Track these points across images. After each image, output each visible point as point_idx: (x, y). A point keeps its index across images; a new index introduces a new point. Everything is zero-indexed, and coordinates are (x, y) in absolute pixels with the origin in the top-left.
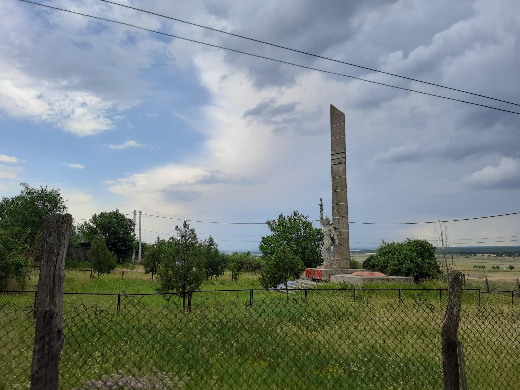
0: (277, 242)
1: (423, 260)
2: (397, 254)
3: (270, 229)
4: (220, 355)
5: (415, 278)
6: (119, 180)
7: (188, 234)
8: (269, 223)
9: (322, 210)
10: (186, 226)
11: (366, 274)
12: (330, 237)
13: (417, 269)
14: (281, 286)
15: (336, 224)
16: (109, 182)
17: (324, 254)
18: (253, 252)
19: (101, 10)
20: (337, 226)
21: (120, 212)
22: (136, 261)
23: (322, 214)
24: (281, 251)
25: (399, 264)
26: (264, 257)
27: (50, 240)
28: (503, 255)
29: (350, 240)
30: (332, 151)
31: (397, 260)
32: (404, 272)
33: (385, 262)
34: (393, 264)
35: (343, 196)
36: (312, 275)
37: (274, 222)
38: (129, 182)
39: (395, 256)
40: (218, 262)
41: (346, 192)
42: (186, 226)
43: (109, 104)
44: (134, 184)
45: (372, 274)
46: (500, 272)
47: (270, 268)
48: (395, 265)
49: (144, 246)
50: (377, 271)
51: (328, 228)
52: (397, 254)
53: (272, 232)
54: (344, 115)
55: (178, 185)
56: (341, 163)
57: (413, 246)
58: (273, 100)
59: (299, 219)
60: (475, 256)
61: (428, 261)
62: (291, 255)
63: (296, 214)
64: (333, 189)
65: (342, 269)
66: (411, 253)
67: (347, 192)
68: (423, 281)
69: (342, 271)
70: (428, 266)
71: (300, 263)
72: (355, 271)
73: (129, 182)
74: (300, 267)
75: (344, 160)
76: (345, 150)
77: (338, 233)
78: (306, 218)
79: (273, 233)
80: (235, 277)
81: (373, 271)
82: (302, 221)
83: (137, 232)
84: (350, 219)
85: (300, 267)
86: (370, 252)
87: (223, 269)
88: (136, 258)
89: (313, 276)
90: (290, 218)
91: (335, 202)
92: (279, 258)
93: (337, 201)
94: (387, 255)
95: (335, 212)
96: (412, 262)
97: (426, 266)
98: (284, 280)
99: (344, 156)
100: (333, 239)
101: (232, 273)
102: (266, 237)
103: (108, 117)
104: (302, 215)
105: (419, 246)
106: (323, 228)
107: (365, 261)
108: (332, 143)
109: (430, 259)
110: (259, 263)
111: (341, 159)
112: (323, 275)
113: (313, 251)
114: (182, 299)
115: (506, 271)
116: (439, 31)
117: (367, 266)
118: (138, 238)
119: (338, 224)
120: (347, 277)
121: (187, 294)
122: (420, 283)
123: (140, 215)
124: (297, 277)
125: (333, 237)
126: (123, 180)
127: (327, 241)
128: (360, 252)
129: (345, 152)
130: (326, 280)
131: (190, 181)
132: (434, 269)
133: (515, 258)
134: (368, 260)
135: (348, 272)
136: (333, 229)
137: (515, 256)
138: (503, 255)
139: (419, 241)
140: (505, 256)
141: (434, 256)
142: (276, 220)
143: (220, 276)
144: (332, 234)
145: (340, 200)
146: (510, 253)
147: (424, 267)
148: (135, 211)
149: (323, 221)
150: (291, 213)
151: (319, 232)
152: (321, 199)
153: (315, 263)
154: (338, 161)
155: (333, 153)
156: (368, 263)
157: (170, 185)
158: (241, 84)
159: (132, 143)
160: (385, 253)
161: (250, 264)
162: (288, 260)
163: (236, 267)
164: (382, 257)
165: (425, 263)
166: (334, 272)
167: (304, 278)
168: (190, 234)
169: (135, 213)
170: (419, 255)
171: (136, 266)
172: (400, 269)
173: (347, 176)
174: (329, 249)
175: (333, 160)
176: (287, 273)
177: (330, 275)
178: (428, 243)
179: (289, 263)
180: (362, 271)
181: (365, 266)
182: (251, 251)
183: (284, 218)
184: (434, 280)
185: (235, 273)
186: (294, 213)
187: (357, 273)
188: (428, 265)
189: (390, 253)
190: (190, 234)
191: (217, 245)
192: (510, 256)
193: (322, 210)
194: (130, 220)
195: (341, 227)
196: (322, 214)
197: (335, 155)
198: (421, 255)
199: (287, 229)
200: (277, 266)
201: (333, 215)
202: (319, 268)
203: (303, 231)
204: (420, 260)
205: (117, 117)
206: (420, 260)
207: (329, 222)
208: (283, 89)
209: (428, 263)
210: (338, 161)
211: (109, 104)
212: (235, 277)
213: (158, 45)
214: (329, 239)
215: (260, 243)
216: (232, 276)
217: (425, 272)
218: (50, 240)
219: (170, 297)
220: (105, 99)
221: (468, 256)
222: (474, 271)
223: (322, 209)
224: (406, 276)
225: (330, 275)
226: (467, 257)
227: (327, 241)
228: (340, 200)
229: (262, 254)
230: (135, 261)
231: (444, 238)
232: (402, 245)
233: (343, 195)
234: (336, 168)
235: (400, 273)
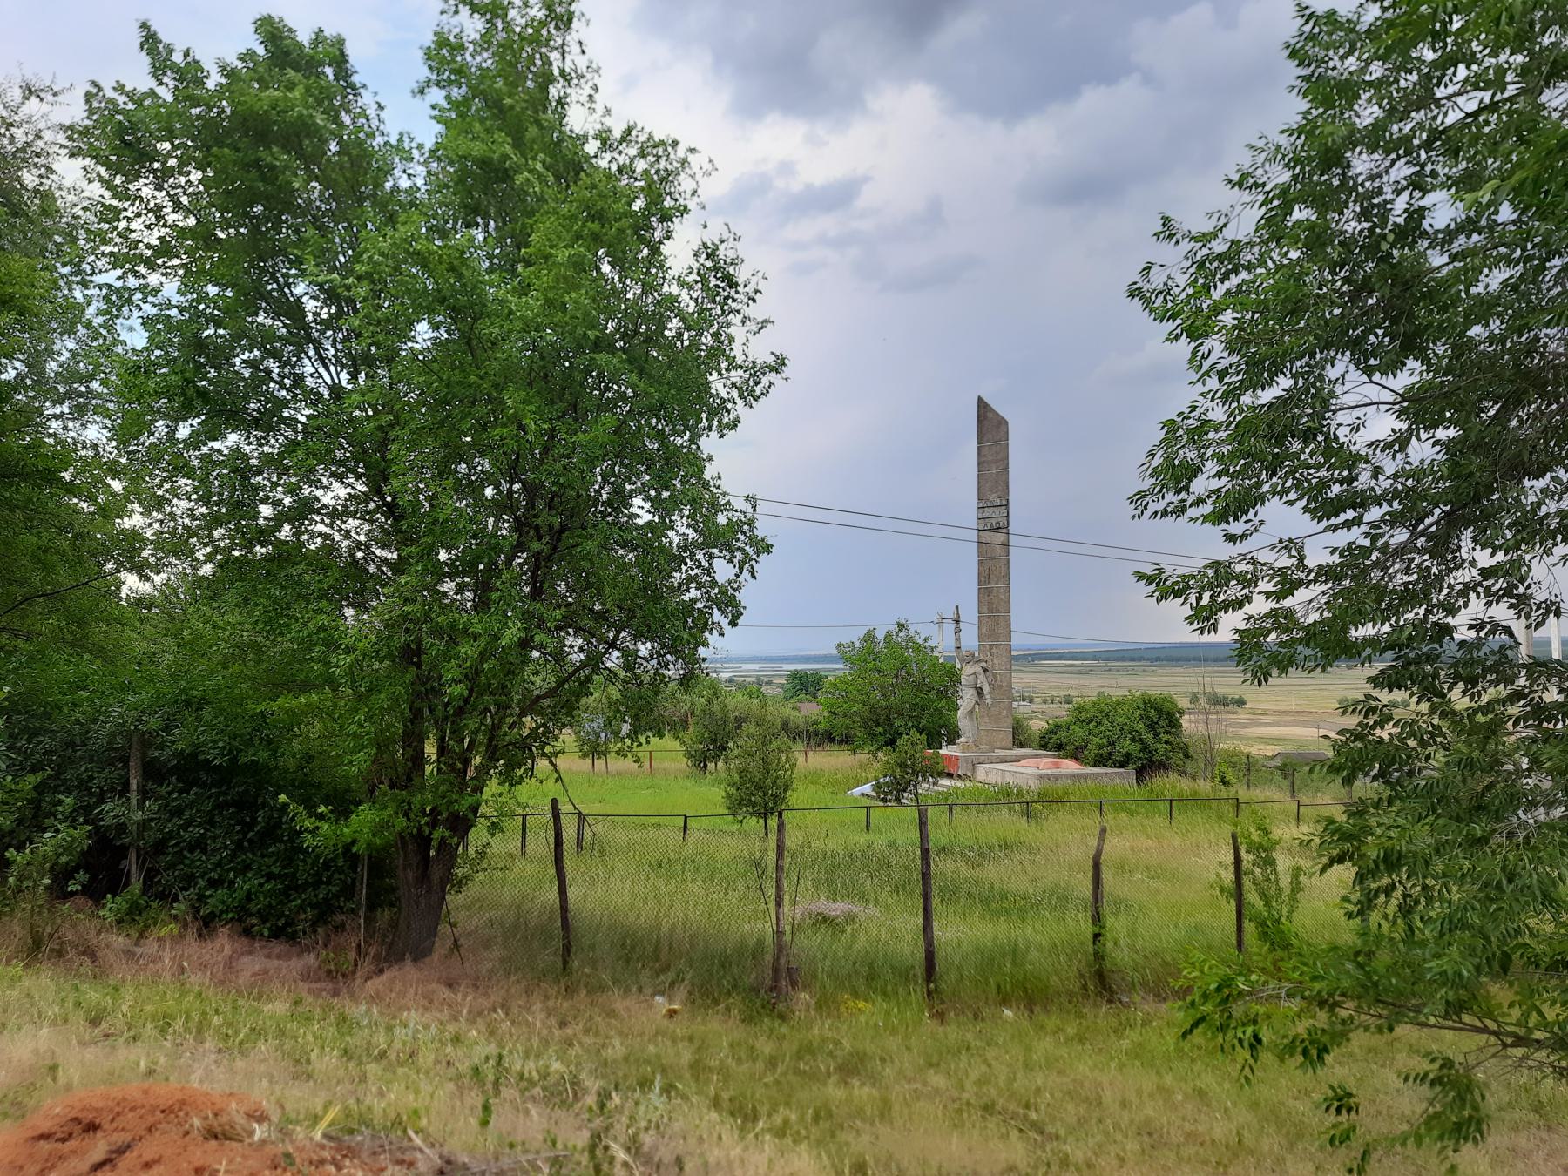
1: (1156, 735)
17: (962, 719)
23: (958, 640)
39: (1102, 728)
45: (1057, 765)
48: (1101, 746)
61: (1165, 737)
63: (901, 627)
64: (979, 582)
95: (984, 631)
96: (1133, 740)
100: (980, 692)
114: (762, 821)
174: (971, 712)
184: (1173, 777)
198: (1152, 727)
204: (1148, 737)
206: (1148, 737)
209: (1166, 742)
214: (972, 692)
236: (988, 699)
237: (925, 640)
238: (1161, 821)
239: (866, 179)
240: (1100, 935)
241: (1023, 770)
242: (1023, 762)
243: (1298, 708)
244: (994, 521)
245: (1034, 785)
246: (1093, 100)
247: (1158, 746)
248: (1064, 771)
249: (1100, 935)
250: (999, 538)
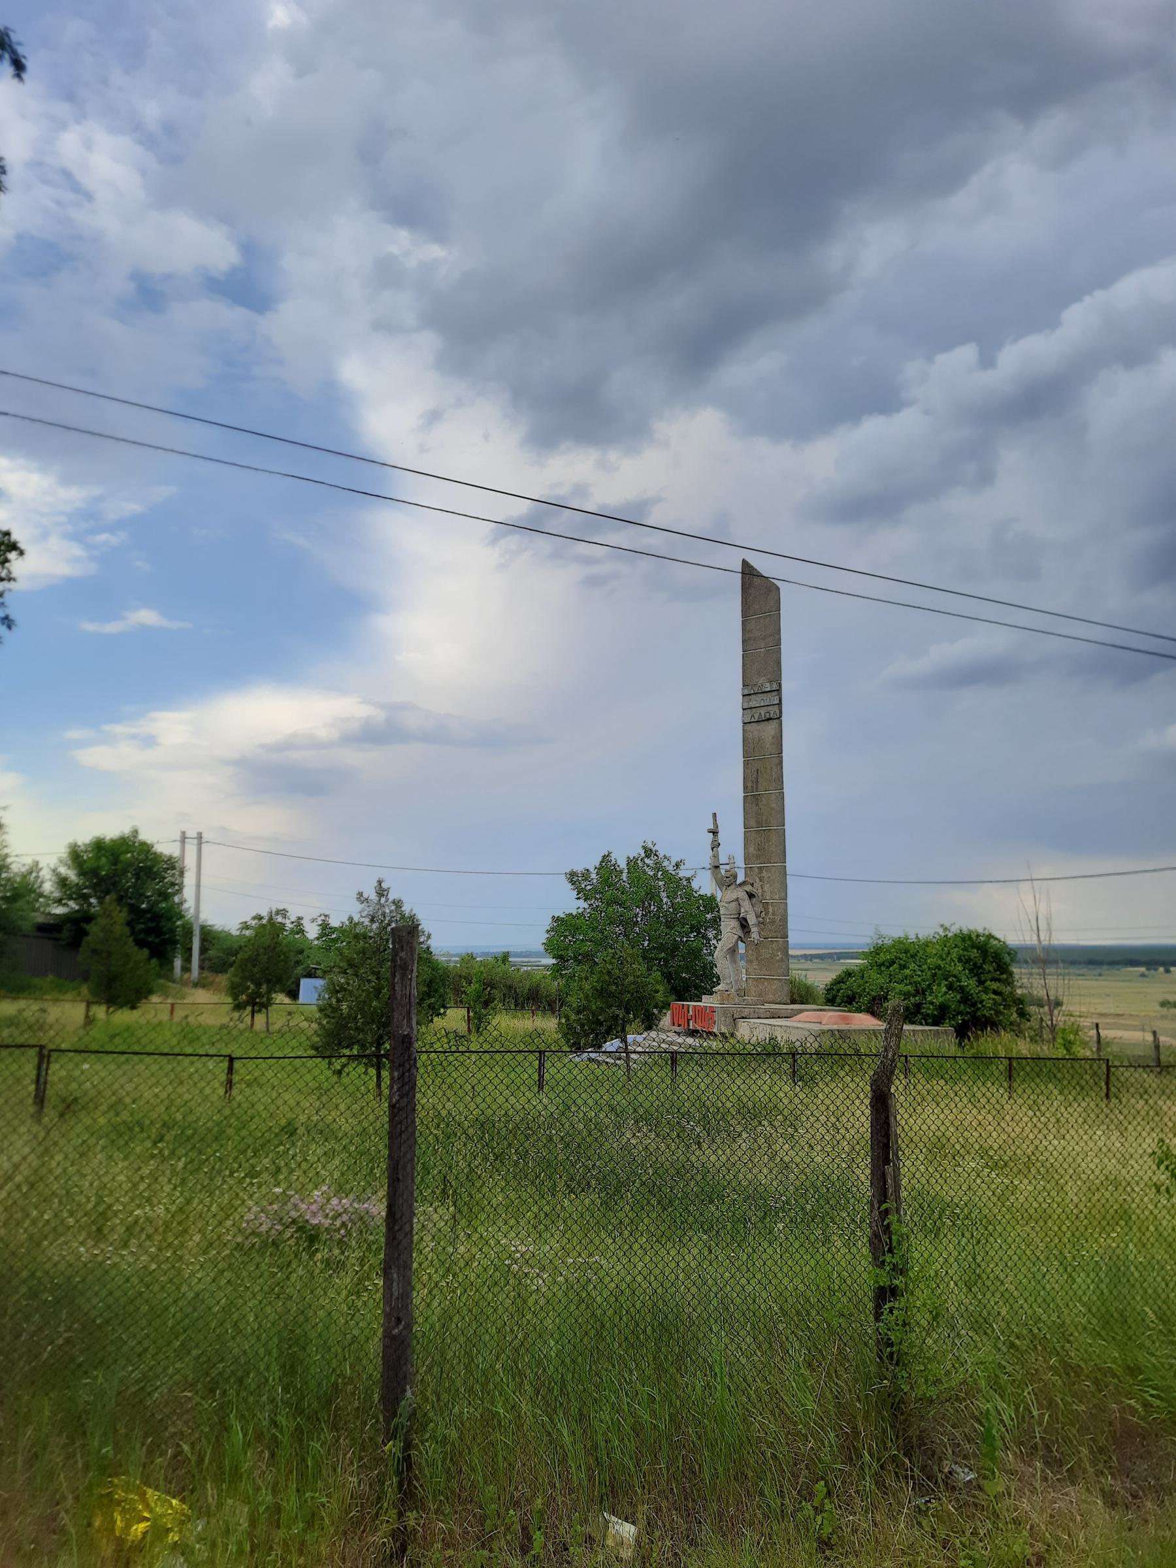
0: (593, 930)
1: (981, 982)
2: (912, 966)
3: (575, 892)
4: (119, 1523)
5: (956, 1031)
6: (106, 728)
7: (388, 911)
8: (573, 878)
9: (715, 845)
10: (381, 892)
11: (830, 1019)
12: (738, 918)
13: (962, 1007)
14: (612, 1045)
15: (752, 885)
16: (74, 734)
17: (723, 966)
18: (522, 952)
19: (59, 203)
20: (756, 890)
21: (143, 836)
22: (186, 975)
23: (716, 857)
24: (612, 957)
25: (917, 993)
26: (557, 970)
27: (403, 954)
29: (790, 925)
31: (911, 984)
32: (928, 1015)
33: (882, 988)
34: (901, 993)
35: (772, 809)
36: (688, 1020)
37: (586, 874)
38: (134, 737)
39: (907, 972)
40: (431, 981)
42: (381, 892)
43: (74, 496)
44: (149, 741)
45: (845, 1019)
47: (587, 997)
48: (907, 995)
49: (209, 936)
50: (859, 1010)
51: (732, 894)
52: (912, 966)
53: (582, 901)
55: (288, 745)
56: (768, 719)
57: (956, 946)
58: (580, 490)
59: (658, 866)
60: (1167, 971)
61: (995, 986)
62: (640, 967)
63: (649, 852)
64: (745, 788)
65: (767, 1006)
66: (950, 965)
68: (977, 1038)
69: (767, 1010)
70: (994, 999)
71: (661, 988)
72: (802, 1011)
73: (134, 737)
74: (660, 997)
75: (778, 711)
76: (780, 685)
77: (759, 908)
78: (677, 865)
79: (583, 904)
80: (477, 1023)
81: (850, 1011)
82: (665, 872)
83: (188, 893)
84: (791, 865)
85: (660, 997)
86: (852, 958)
87: (444, 1001)
88: (186, 969)
89: (691, 1022)
90: (632, 863)
91: (753, 823)
92: (609, 973)
93: (757, 822)
94: (888, 967)
95: (752, 850)
96: (950, 987)
97: (988, 999)
98: (617, 1029)
99: (777, 702)
100: (744, 924)
101: (468, 1013)
102: (562, 916)
103: (76, 537)
104: (665, 857)
105: (973, 947)
106: (719, 895)
107: (832, 984)
108: (744, 665)
109: (999, 980)
110: (538, 986)
112: (716, 1019)
113: (695, 954)
114: (372, 1071)
116: (1075, 295)
117: (834, 997)
118: (192, 911)
119: (758, 884)
120: (781, 1026)
121: (384, 1060)
122: (966, 1041)
123: (200, 844)
124: (650, 1023)
125: (745, 919)
126: (119, 729)
127: (729, 928)
128: (830, 956)
130: (723, 1034)
131: (323, 734)
132: (1007, 1007)
134: (839, 981)
135: (783, 1012)
136: (746, 897)
139: (970, 931)
141: (1011, 974)
142: (592, 869)
143: (435, 1019)
144: (743, 910)
145: (764, 818)
147: (981, 1002)
148: (183, 833)
149: (719, 876)
150: (637, 851)
151: (710, 903)
152: (715, 815)
153: (697, 987)
155: (746, 692)
156: (838, 991)
157: (263, 746)
158: (486, 437)
159: (147, 616)
160: (883, 964)
161: (510, 987)
162: (631, 978)
163: (479, 997)
164: (873, 974)
165: (986, 990)
166: (746, 1012)
167: (666, 1028)
168: (391, 912)
169: (184, 838)
170: (971, 971)
171: (186, 990)
172: (918, 1006)
173: (784, 754)
174: (733, 951)
175: (749, 711)
176: (628, 1013)
177: (734, 1020)
178: (996, 939)
179: (633, 986)
180: (821, 1010)
181: (830, 996)
182: (475, 951)
183: (613, 862)
184: (1006, 1036)
185: (475, 1013)
187: (807, 1016)
188: (994, 996)
189: (894, 963)
190: (391, 912)
191: (429, 937)
193: (715, 845)
194: (171, 858)
195: (767, 892)
196: (716, 857)
197: (753, 696)
198: (976, 970)
199: (622, 893)
200: (601, 993)
201: (747, 859)
202: (707, 1001)
203: (665, 900)
204: (970, 983)
205: (103, 537)
206: (970, 983)
207: (735, 877)
208: (613, 455)
209: (995, 992)
211: (74, 496)
212: (477, 1023)
213: (232, 316)
214: (734, 923)
215: (548, 932)
216: (469, 1020)
217: (984, 1016)
218: (403, 954)
219: (344, 1066)
220: (66, 480)
221: (1147, 973)
222: (1163, 1017)
223: (716, 843)
224: (935, 1024)
225: (734, 1020)
226: (1143, 975)
227: (729, 928)
229: (551, 961)
230: (182, 976)
231: (1043, 926)
232: (927, 944)
234: (756, 733)
235: (920, 1016)
236: (755, 934)
237: (677, 865)
238: (997, 1092)
239: (658, 500)
240: (894, 1292)
241: (799, 1025)
242: (795, 1018)
243: (1119, 1011)
244: (763, 711)
245: (811, 1041)
246: (874, 427)
247: (984, 997)
248: (854, 1027)
249: (894, 1292)
250: (770, 728)
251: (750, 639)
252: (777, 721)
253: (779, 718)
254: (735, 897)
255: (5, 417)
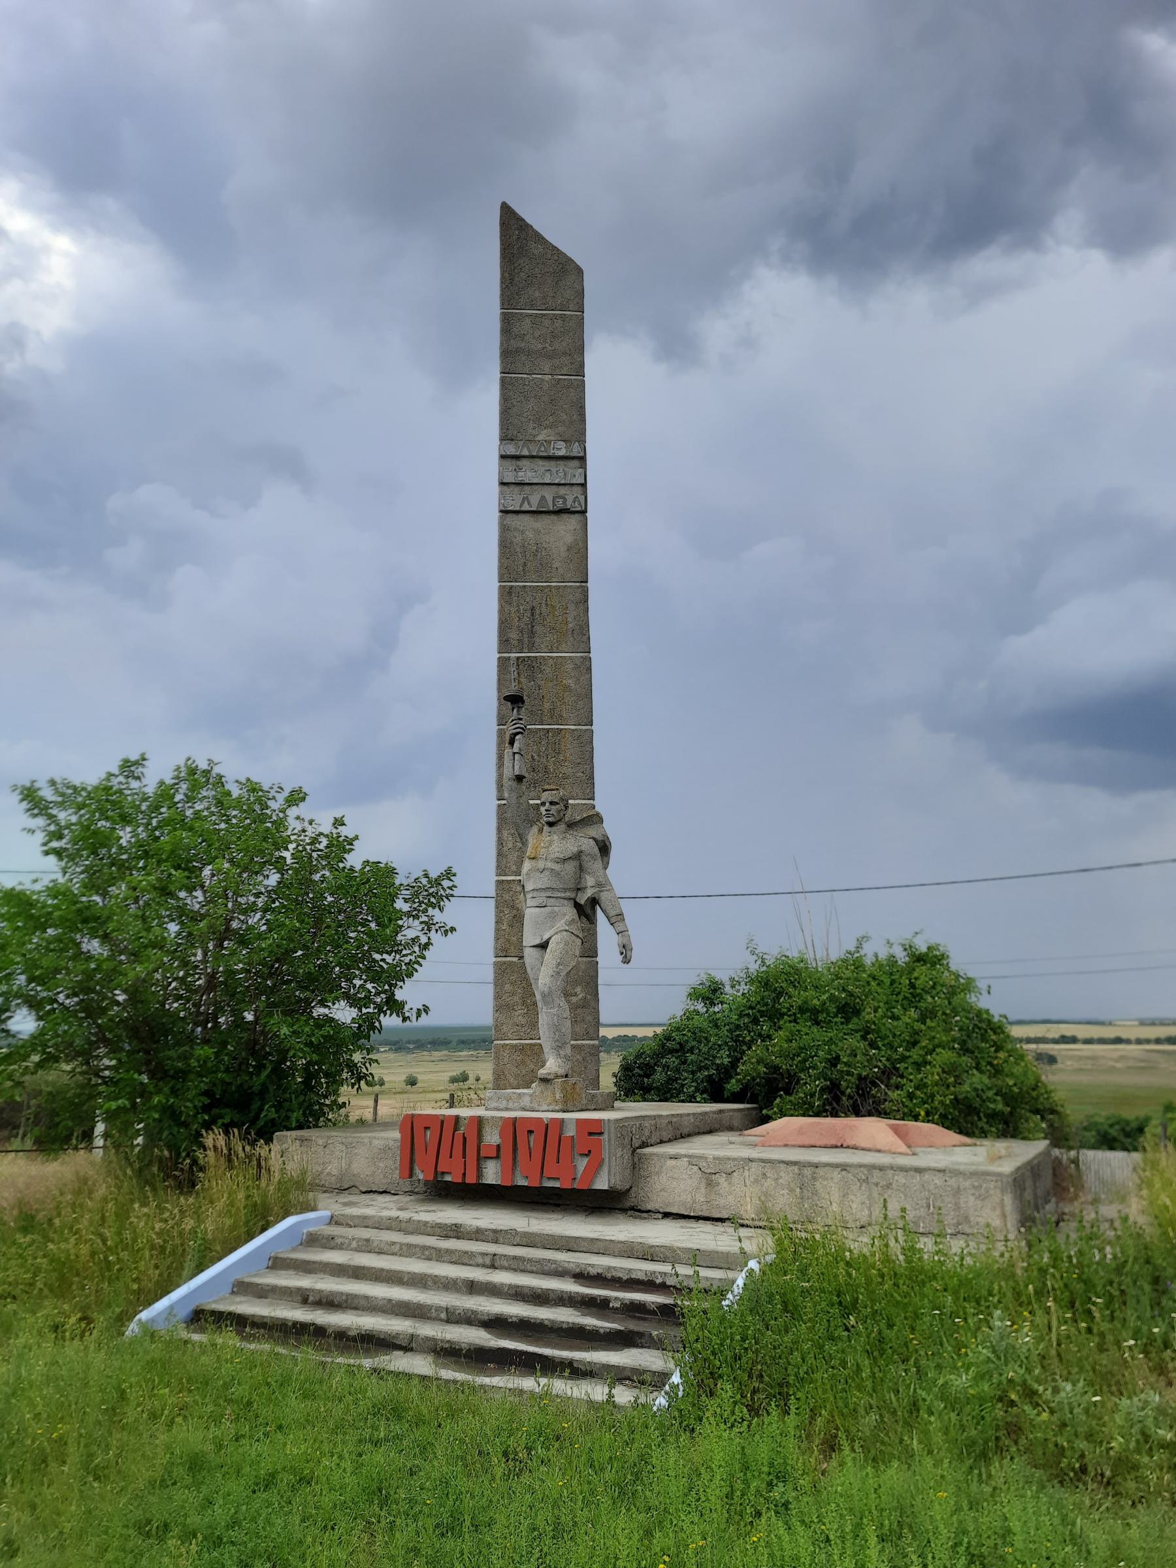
28: (382, 1050)
30: (505, 438)
35: (567, 688)
41: (585, 667)
46: (387, 1094)
54: (580, 272)
64: (504, 643)
67: (589, 669)
75: (582, 498)
111: (562, 491)
115: (399, 1093)
129: (582, 459)
133: (410, 1057)
137: (409, 1051)
138: (382, 1050)
140: (385, 1051)
145: (547, 706)
146: (395, 1043)
154: (543, 498)
155: (511, 450)
186: (14, 790)
187: (801, 1131)
192: (397, 1050)
210: (543, 498)
228: (547, 706)
233: (570, 682)
244: (548, 494)
251: (518, 351)
252: (577, 516)
253: (584, 512)
254: (575, 850)
255: (1172, 857)
